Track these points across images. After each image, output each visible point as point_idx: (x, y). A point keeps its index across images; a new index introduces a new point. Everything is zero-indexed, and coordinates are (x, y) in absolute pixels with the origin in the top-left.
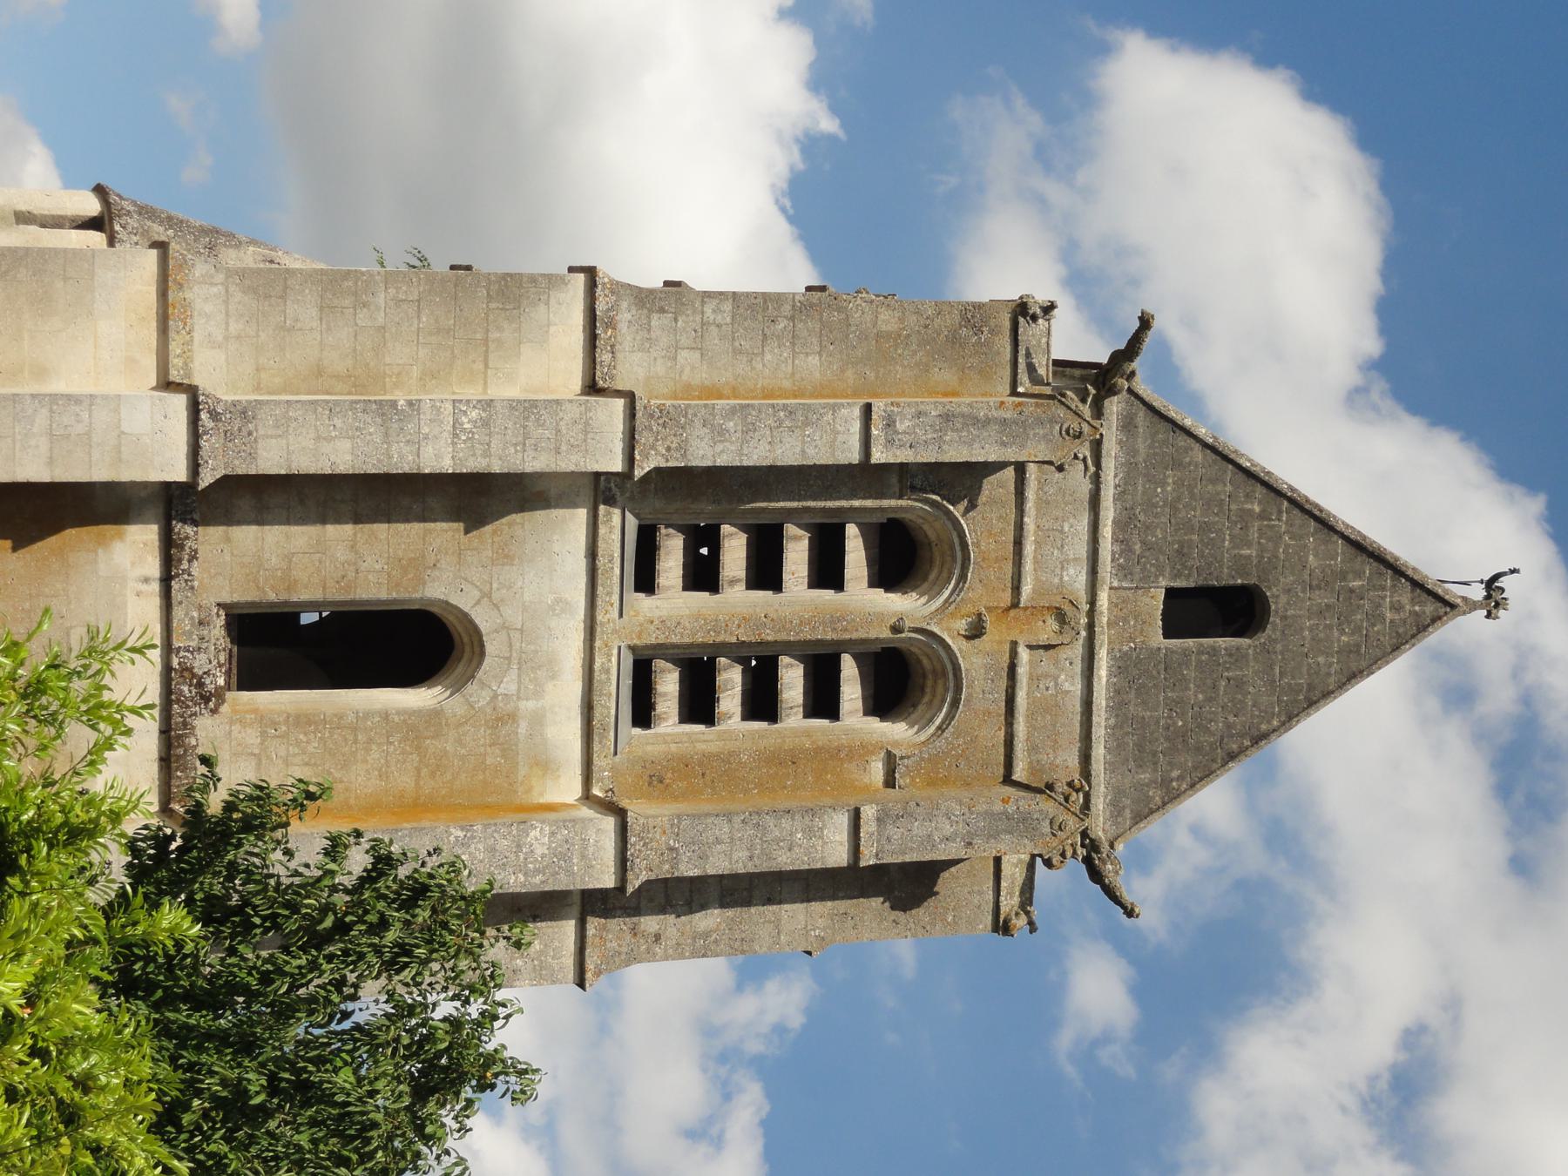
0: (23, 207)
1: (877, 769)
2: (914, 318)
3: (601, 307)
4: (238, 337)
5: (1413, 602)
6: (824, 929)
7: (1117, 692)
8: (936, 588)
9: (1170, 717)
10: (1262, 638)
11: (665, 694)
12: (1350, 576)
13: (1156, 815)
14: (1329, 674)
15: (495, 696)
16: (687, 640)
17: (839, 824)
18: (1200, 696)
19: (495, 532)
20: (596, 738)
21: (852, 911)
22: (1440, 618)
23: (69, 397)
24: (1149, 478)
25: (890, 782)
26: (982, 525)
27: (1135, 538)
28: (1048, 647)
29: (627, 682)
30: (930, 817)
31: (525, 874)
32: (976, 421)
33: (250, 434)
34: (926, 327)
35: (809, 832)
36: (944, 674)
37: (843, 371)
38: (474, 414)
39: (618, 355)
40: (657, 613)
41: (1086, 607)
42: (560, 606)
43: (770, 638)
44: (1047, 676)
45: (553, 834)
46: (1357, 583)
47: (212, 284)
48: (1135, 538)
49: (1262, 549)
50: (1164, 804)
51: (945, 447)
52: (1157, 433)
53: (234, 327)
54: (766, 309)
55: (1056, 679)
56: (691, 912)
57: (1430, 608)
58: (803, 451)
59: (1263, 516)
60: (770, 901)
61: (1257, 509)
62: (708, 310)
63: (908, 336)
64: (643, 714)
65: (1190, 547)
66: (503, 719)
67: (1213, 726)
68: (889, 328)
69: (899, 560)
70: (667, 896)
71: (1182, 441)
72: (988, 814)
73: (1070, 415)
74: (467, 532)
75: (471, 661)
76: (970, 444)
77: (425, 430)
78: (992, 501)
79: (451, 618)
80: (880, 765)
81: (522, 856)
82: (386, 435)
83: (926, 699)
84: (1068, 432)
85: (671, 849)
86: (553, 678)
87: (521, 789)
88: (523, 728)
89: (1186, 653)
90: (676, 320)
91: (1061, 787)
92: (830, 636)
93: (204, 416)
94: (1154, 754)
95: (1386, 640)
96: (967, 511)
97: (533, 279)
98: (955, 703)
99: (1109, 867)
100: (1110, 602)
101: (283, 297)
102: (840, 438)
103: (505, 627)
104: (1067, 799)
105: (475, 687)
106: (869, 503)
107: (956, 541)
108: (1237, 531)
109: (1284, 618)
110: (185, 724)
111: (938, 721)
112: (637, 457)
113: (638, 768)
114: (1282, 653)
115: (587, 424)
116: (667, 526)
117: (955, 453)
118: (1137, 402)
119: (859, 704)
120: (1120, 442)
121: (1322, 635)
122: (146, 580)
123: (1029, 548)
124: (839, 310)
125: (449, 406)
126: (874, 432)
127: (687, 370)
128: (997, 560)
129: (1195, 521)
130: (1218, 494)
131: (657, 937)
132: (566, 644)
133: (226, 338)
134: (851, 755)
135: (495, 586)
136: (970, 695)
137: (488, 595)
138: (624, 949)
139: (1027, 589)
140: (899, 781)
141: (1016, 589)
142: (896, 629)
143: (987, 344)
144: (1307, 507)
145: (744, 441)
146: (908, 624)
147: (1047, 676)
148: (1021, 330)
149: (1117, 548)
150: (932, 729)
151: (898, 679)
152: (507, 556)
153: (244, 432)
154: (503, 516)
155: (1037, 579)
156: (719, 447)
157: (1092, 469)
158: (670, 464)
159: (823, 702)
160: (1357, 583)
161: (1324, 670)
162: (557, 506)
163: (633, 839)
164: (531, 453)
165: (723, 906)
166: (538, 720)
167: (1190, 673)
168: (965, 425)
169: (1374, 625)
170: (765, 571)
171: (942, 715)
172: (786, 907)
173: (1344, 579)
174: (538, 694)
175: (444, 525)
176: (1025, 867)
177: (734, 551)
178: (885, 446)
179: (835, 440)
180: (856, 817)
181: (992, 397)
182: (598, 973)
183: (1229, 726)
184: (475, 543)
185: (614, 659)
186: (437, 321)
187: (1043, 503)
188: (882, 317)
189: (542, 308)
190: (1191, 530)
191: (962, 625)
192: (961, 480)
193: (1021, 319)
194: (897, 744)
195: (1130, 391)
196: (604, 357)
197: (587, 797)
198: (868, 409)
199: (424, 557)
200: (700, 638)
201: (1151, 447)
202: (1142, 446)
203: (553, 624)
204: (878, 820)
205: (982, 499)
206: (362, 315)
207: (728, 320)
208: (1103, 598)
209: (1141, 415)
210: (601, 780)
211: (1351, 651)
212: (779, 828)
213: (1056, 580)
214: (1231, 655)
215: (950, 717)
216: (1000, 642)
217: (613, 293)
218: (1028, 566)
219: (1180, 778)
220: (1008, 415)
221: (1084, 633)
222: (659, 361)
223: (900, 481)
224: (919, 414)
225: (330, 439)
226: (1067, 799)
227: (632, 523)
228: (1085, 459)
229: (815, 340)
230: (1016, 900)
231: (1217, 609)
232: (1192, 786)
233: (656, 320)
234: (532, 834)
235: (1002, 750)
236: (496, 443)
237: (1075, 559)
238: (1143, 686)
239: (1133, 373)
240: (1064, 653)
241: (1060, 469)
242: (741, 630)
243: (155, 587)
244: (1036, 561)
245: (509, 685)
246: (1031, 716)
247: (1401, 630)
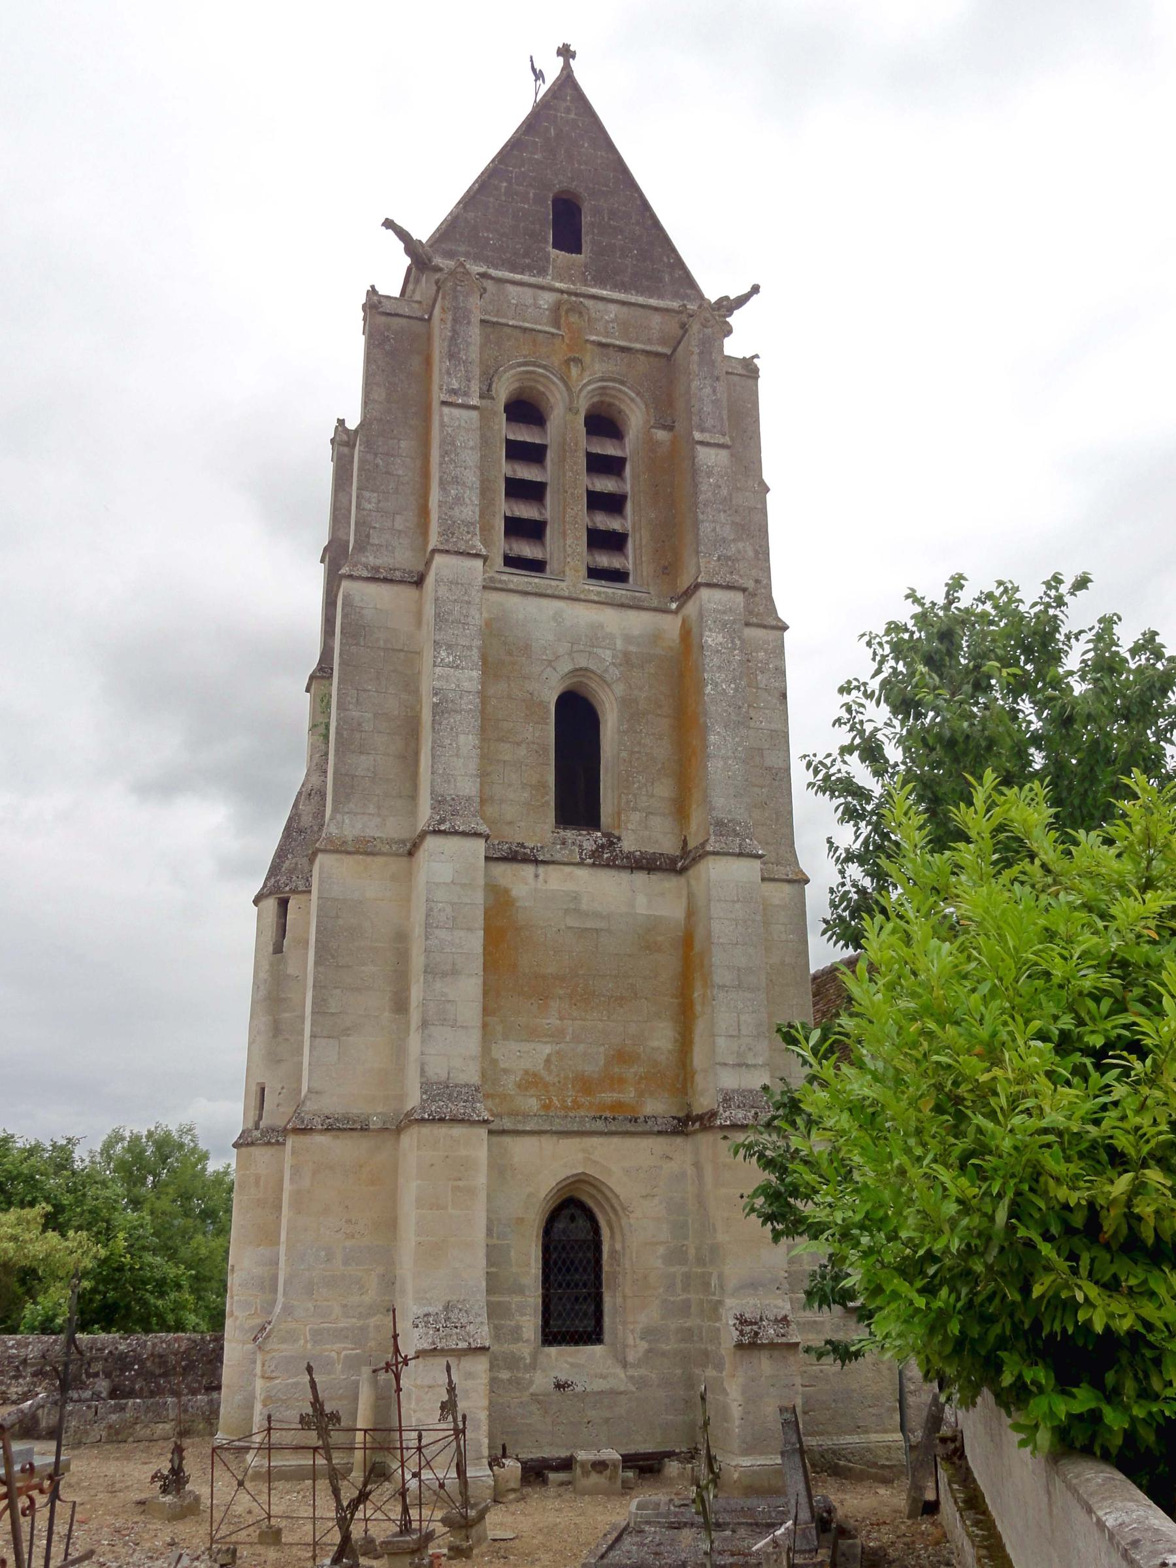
0: (271, 949)
3: (365, 574)
4: (379, 808)
5: (565, 100)
7: (616, 287)
15: (613, 664)
23: (428, 916)
30: (701, 400)
33: (453, 799)
35: (709, 474)
36: (604, 388)
38: (443, 654)
42: (557, 617)
44: (606, 328)
45: (710, 630)
47: (343, 822)
53: (372, 809)
55: (607, 322)
61: (505, 184)
62: (369, 506)
66: (627, 660)
67: (638, 233)
68: (384, 395)
76: (468, 344)
77: (453, 686)
82: (456, 712)
83: (617, 403)
85: (719, 559)
93: (442, 828)
101: (353, 777)
110: (627, 858)
115: (451, 583)
122: (537, 876)
125: (438, 670)
132: (582, 615)
133: (379, 815)
147: (606, 328)
153: (452, 803)
156: (467, 500)
166: (628, 639)
189: (365, 612)
196: (398, 575)
199: (524, 700)
206: (366, 727)
225: (458, 748)
229: (391, 442)
231: (566, 224)
236: (462, 642)
243: (542, 869)
245: (607, 655)
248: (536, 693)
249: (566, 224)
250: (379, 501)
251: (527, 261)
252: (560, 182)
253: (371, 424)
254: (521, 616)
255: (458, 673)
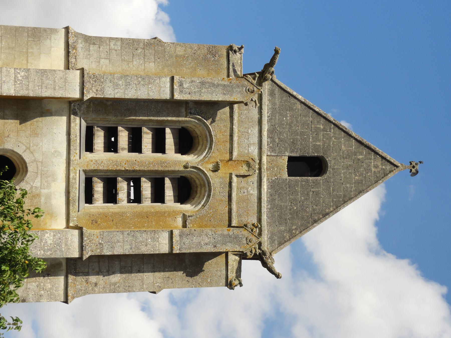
1: (179, 221)
2: (190, 50)
3: (71, 41)
6: (160, 283)
7: (271, 195)
8: (200, 153)
9: (291, 206)
10: (325, 176)
11: (98, 191)
12: (358, 154)
13: (287, 243)
14: (351, 191)
15: (32, 187)
16: (105, 168)
17: (165, 236)
18: (303, 198)
19: (31, 124)
20: (71, 204)
21: (171, 277)
22: (392, 171)
24: (281, 114)
25: (184, 226)
26: (218, 128)
27: (276, 137)
28: (244, 176)
29: (83, 185)
30: (200, 235)
31: (44, 251)
32: (213, 85)
34: (195, 53)
35: (153, 239)
36: (204, 186)
37: (163, 69)
38: (22, 74)
39: (78, 60)
40: (94, 158)
41: (258, 161)
43: (137, 169)
44: (244, 188)
45: (54, 235)
46: (361, 157)
48: (276, 137)
49: (324, 143)
50: (290, 239)
51: (202, 94)
52: (283, 97)
54: (134, 45)
55: (247, 189)
56: (109, 275)
57: (389, 167)
58: (148, 94)
59: (324, 130)
60: (139, 271)
61: (322, 127)
62: (112, 45)
63: (188, 57)
64: (89, 199)
65: (297, 141)
68: (180, 53)
69: (186, 143)
70: (99, 268)
71: (293, 100)
72: (222, 235)
73: (249, 84)
74: (20, 124)
75: (22, 174)
77: (4, 79)
78: (221, 120)
79: (15, 158)
80: (181, 219)
81: (42, 244)
83: (198, 195)
84: (249, 91)
85: (100, 244)
86: (54, 181)
87: (42, 224)
88: (43, 200)
89: (296, 181)
90: (99, 48)
91: (250, 226)
92: (160, 169)
94: (286, 220)
95: (372, 179)
96: (212, 123)
97: (45, 30)
98: (209, 196)
99: (269, 260)
100: (267, 161)
102: (162, 89)
103: (35, 161)
104: (252, 230)
105: (24, 183)
106: (174, 119)
107: (208, 134)
108: (314, 135)
109: (333, 169)
111: (202, 203)
112: (85, 92)
113: (87, 217)
114: (333, 182)
115: (65, 79)
116: (97, 127)
117: (206, 96)
118: (275, 85)
119: (173, 147)
120: (269, 100)
121: (348, 176)
123: (235, 138)
124: (161, 46)
125: (13, 70)
126: (175, 87)
127: (104, 66)
128: (223, 142)
129: (298, 131)
130: (307, 121)
131: (96, 284)
134: (169, 215)
135: (31, 145)
136: (214, 194)
137: (28, 148)
138: (83, 289)
139: (235, 154)
140: (188, 225)
141: (231, 153)
142: (186, 167)
143: (218, 61)
144: (341, 127)
145: (126, 89)
146: (190, 165)
147: (244, 188)
148: (230, 56)
149: (269, 140)
150: (200, 206)
151: (186, 189)
152: (36, 134)
154: (34, 118)
155: (239, 151)
156: (116, 91)
157: (258, 105)
158: (97, 96)
159: (158, 196)
160: (361, 157)
161: (349, 190)
162: (55, 115)
163: (85, 239)
164: (44, 89)
165: (121, 273)
166: (49, 197)
167: (299, 189)
168: (210, 86)
169: (368, 173)
170: (135, 146)
171: (204, 201)
172: (145, 274)
173: (356, 155)
174: (49, 187)
175: (12, 121)
176: (237, 262)
177: (123, 138)
178: (180, 93)
179: (160, 90)
180: (171, 233)
181: (220, 78)
182: (73, 298)
183: (314, 210)
184: (24, 128)
185: (78, 175)
186: (8, 44)
187: (241, 122)
188: (178, 49)
189: (48, 41)
190: (297, 134)
191: (211, 166)
192: (209, 108)
193: (230, 52)
194: (187, 211)
195: (272, 80)
197: (68, 227)
198: (172, 79)
199: (4, 132)
200: (110, 168)
201: (281, 102)
202: (277, 101)
203: (54, 160)
204: (180, 236)
205: (217, 118)
207: (119, 48)
208: (264, 159)
209: (277, 89)
210: (73, 221)
211: (359, 182)
212: (141, 237)
213: (246, 151)
214: (314, 183)
215: (207, 201)
216: (225, 173)
217: (75, 36)
218: (235, 145)
219: (296, 229)
220: (226, 83)
221: (257, 171)
222: (93, 63)
223: (186, 111)
224: (192, 81)
226: (252, 230)
227: (84, 124)
228: (255, 101)
229: (152, 57)
230: (234, 275)
231: (308, 166)
232: (301, 232)
233: (92, 47)
234: (47, 235)
235: (227, 215)
237: (253, 144)
238: (281, 193)
239: (273, 72)
240: (250, 179)
241: (246, 104)
242: (126, 165)
244: (238, 144)
245: (37, 183)
246: (238, 203)
247: (378, 175)
248: (9, 139)
249: (308, 166)
250: (116, 50)
251: (277, 140)
252: (331, 162)
253: (161, 46)
254: (55, 131)
255: (12, 82)
